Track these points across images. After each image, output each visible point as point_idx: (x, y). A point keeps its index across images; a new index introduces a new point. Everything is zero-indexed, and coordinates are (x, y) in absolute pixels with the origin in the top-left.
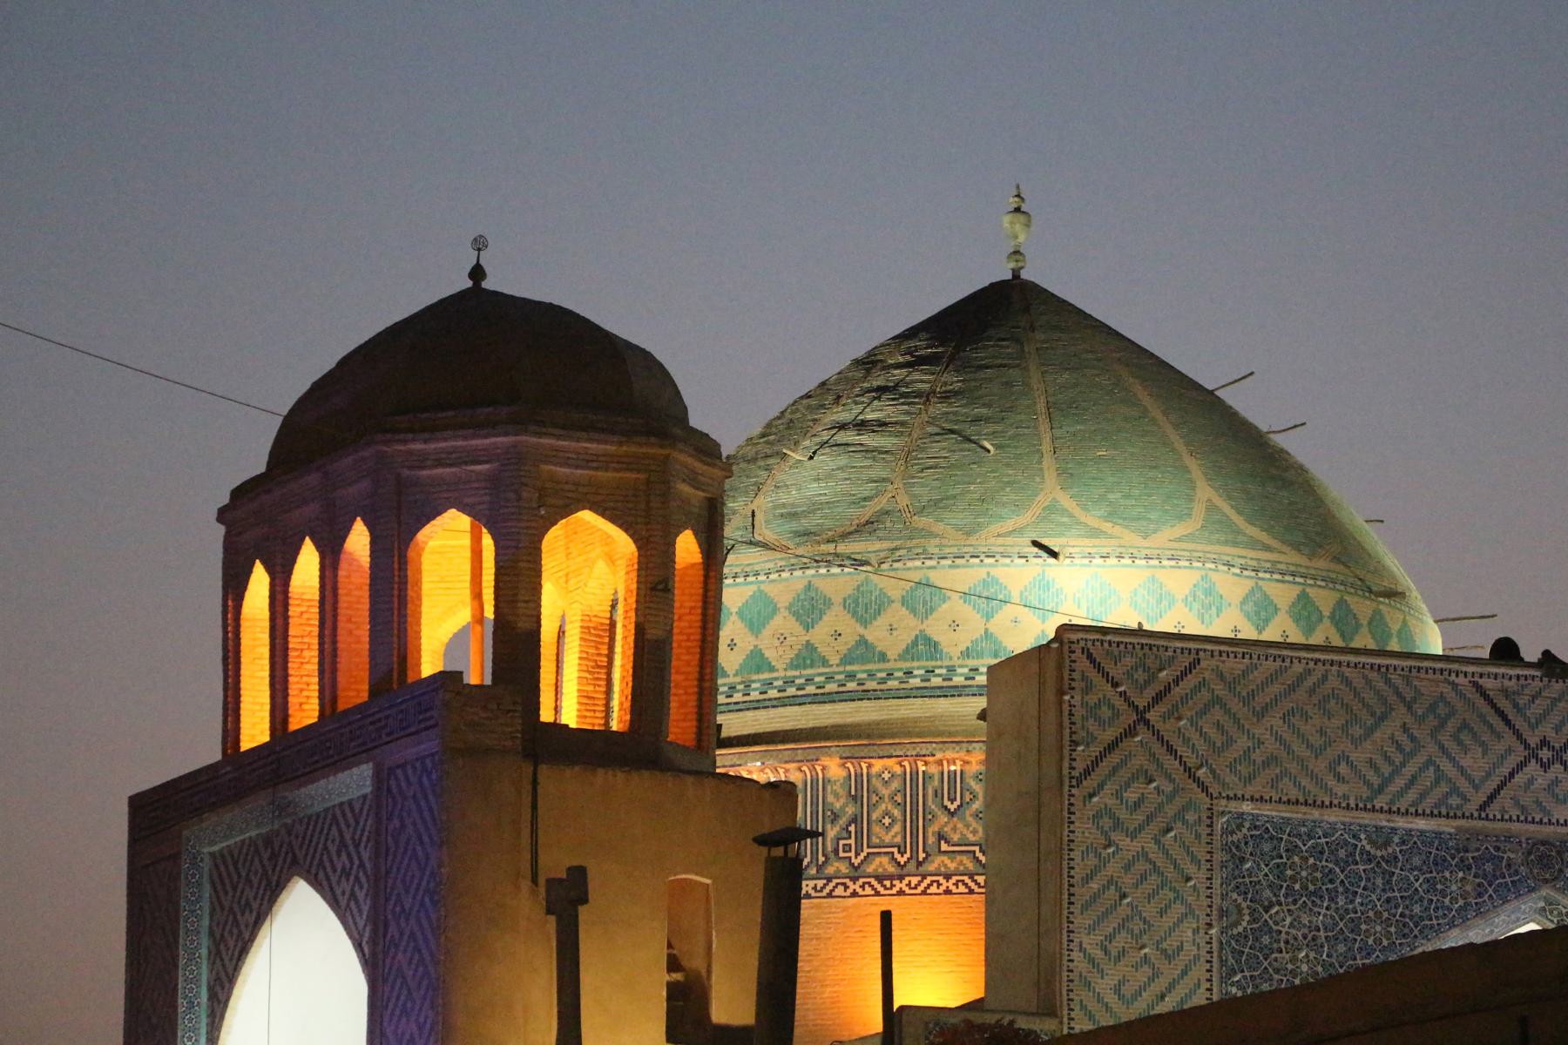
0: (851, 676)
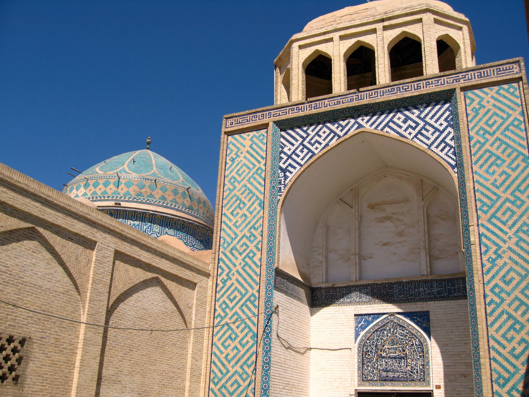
0: (148, 200)
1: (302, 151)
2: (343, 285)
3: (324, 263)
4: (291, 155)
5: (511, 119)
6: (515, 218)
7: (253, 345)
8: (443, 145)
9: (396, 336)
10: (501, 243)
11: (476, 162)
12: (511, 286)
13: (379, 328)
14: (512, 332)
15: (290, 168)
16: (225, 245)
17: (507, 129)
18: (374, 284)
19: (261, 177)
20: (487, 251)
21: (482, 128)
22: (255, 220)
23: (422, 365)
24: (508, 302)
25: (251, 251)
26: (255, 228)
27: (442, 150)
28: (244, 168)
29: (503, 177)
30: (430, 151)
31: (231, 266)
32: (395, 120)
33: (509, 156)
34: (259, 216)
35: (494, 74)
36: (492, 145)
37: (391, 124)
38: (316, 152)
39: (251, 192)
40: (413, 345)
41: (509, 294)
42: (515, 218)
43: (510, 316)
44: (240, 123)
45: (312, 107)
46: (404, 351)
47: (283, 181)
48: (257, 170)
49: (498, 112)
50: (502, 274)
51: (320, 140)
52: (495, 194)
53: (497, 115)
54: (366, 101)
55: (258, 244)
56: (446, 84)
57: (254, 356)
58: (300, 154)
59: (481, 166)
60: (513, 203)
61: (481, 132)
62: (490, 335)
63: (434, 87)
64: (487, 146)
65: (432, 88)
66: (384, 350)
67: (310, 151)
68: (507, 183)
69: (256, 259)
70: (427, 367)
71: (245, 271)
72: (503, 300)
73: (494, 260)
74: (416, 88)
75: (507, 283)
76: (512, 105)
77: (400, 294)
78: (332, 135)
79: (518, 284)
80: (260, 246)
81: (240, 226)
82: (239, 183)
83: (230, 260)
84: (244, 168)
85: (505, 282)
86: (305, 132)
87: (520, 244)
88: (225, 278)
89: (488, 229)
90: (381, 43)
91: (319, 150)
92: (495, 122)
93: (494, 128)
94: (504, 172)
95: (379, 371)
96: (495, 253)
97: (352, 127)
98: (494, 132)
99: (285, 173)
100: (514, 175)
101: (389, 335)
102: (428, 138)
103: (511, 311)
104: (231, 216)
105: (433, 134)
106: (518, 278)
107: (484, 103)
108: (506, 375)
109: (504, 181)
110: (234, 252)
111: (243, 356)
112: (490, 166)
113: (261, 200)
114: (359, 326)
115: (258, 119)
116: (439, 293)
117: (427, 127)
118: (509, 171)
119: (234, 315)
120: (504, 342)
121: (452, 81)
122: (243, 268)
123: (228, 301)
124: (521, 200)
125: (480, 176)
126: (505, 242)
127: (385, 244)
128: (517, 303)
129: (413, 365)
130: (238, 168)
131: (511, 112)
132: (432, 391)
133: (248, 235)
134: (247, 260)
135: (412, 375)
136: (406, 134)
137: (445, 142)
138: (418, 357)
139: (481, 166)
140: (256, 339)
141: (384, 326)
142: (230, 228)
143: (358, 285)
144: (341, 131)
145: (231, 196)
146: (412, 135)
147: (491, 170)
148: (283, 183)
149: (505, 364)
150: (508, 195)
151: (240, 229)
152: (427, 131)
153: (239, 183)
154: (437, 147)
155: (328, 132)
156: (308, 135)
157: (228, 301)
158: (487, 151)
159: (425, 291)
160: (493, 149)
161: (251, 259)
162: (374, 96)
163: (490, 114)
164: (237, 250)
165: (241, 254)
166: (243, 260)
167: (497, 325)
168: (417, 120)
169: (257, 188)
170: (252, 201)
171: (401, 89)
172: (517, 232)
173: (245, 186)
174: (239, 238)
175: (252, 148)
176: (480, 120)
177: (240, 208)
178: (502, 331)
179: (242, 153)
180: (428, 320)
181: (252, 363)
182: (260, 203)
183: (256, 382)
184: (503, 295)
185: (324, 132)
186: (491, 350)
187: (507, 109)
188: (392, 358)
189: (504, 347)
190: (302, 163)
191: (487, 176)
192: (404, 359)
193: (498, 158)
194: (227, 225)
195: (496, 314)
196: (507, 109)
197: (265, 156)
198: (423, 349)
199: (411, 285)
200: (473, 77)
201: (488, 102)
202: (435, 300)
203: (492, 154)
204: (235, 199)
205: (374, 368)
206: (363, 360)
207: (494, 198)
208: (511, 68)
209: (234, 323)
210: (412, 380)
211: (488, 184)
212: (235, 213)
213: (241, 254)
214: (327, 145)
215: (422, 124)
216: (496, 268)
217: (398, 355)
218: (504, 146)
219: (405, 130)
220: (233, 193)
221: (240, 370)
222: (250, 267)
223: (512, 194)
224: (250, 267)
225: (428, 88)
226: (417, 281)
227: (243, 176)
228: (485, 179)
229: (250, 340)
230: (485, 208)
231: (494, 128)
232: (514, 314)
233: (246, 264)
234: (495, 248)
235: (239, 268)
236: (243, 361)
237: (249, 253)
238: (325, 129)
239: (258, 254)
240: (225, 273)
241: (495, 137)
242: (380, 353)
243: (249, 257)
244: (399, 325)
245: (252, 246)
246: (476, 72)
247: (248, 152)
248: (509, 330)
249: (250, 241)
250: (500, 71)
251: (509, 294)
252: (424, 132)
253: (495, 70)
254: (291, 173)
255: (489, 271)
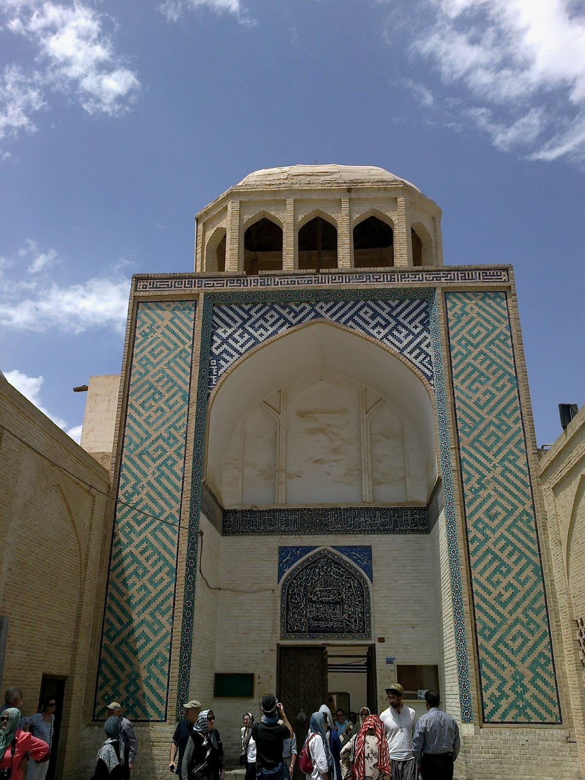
1: (241, 336)
2: (265, 509)
3: (240, 479)
4: (227, 338)
5: (496, 332)
6: (500, 445)
7: (169, 584)
8: (417, 351)
9: (330, 576)
10: (485, 472)
11: (457, 376)
12: (496, 522)
13: (309, 565)
14: (498, 575)
15: (224, 355)
16: (132, 447)
17: (492, 342)
18: (305, 509)
19: (185, 362)
20: (469, 479)
21: (464, 338)
22: (177, 417)
23: (361, 613)
24: (493, 540)
25: (170, 457)
26: (175, 428)
27: (416, 357)
28: (162, 347)
29: (488, 397)
30: (402, 356)
31: (139, 475)
32: (361, 313)
33: (494, 373)
34: (182, 412)
35: (480, 279)
36: (475, 359)
37: (356, 318)
38: (261, 339)
39: (171, 380)
40: (350, 587)
41: (494, 531)
42: (500, 445)
43: (496, 557)
44: (157, 288)
45: (257, 283)
46: (339, 594)
47: (215, 370)
48: (181, 352)
49: (483, 322)
50: (486, 506)
51: (267, 325)
52: (478, 414)
53: (482, 325)
54: (327, 286)
55: (179, 448)
56: (424, 281)
57: (172, 599)
58: (239, 339)
59: (463, 381)
60: (498, 427)
61: (463, 342)
62: (473, 578)
63: (410, 282)
64: (469, 359)
65: (400, 284)
66: (315, 593)
67: (252, 336)
68: (492, 404)
69: (177, 469)
70: (368, 615)
71: (161, 483)
72: (487, 538)
73: (477, 491)
74: (389, 280)
75: (492, 518)
76: (499, 317)
77: (337, 523)
78: (282, 321)
79: (504, 520)
80: (182, 452)
81: (154, 423)
82: (154, 366)
83: (138, 468)
84: (162, 347)
85: (489, 517)
86: (247, 312)
87: (505, 474)
88: (131, 491)
89: (470, 455)
90: (289, 220)
91: (264, 337)
92: (479, 333)
93: (478, 339)
94: (488, 391)
95: (308, 620)
96: (478, 482)
97: (307, 315)
98: (478, 344)
99: (218, 360)
100: (499, 395)
101: (322, 574)
102: (401, 342)
103: (497, 551)
104: (140, 409)
105: (406, 336)
106: (504, 514)
107: (467, 309)
108: (492, 626)
109: (488, 401)
110: (145, 457)
111: (154, 599)
112: (473, 383)
113: (184, 391)
114: (284, 561)
115: (183, 286)
116: (382, 525)
117: (400, 328)
118: (494, 391)
119: (142, 542)
120: (490, 587)
121: (431, 279)
122: (157, 480)
123: (133, 523)
124: (507, 425)
125: (462, 392)
126: (489, 470)
127: (316, 462)
128: (503, 542)
129: (350, 613)
130: (152, 346)
131: (496, 324)
132: (374, 645)
133: (166, 436)
134: (164, 468)
135: (349, 625)
136: (374, 332)
137: (420, 349)
138: (357, 603)
139: (463, 381)
140: (174, 575)
141: (315, 562)
142: (139, 425)
143: (284, 510)
144: (294, 317)
145: (141, 382)
146: (382, 335)
147: (474, 387)
148: (215, 373)
149: (492, 613)
150: (492, 417)
151: (155, 427)
152: (400, 333)
153: (154, 366)
154: (411, 353)
155: (277, 316)
156: (251, 317)
157: (133, 523)
158: (469, 364)
159: (366, 521)
160: (476, 364)
161: (170, 467)
162: (337, 281)
163: (473, 323)
164: (148, 454)
165: (154, 461)
166: (158, 468)
167: (481, 566)
168: (387, 317)
169: (179, 376)
170: (172, 391)
171: (371, 278)
172: (503, 460)
173: (163, 372)
174: (152, 438)
175: (174, 323)
176: (463, 328)
177: (155, 400)
178: (487, 574)
179: (158, 327)
180: (370, 557)
181: (168, 609)
182: (184, 396)
183: (174, 634)
184: (488, 532)
185: (272, 316)
186: (474, 595)
187: (493, 321)
188: (325, 603)
189: (490, 593)
190: (242, 350)
191: (470, 394)
192: (339, 604)
193: (482, 374)
194: (135, 420)
195: (480, 553)
196: (493, 321)
197: (191, 336)
198: (363, 593)
199: (350, 513)
200: (456, 277)
201: (472, 309)
202: (378, 534)
203: (475, 369)
204: (146, 387)
205: (302, 616)
206: (288, 605)
207: (477, 419)
208: (499, 274)
209: (142, 553)
210: (350, 631)
211: (470, 403)
212: (147, 405)
213: (154, 461)
214: (275, 332)
215: (394, 323)
216: (480, 500)
217: (333, 600)
218: (488, 362)
219: (373, 328)
220: (145, 378)
221: (149, 618)
222: (168, 478)
223: (497, 416)
224: (168, 478)
225: (403, 282)
226: (358, 508)
227: (160, 358)
228: (468, 397)
229: (165, 577)
230: (467, 430)
231: (478, 339)
232: (499, 553)
233: (163, 474)
234: (478, 476)
235: (151, 478)
236: (153, 606)
237: (167, 460)
238: (272, 312)
239: (181, 463)
240: (131, 484)
241: (479, 350)
242: (310, 597)
243: (167, 465)
244: (334, 561)
245: (170, 451)
246: (459, 273)
247: (167, 327)
248: (494, 572)
249: (168, 444)
250: (486, 276)
251: (494, 531)
252: (395, 332)
253: (481, 274)
254: (227, 362)
255: (471, 503)
